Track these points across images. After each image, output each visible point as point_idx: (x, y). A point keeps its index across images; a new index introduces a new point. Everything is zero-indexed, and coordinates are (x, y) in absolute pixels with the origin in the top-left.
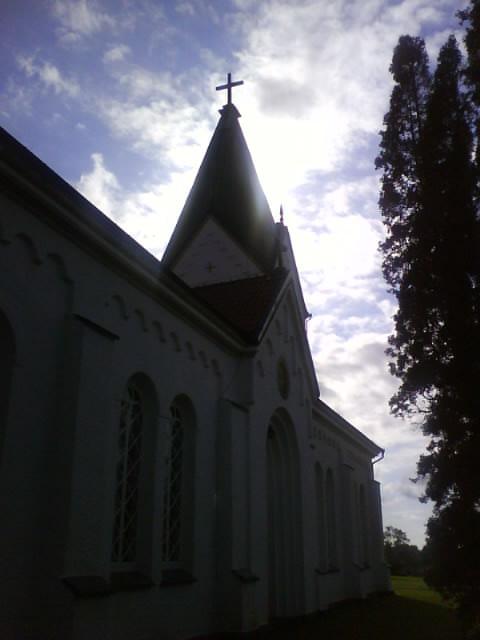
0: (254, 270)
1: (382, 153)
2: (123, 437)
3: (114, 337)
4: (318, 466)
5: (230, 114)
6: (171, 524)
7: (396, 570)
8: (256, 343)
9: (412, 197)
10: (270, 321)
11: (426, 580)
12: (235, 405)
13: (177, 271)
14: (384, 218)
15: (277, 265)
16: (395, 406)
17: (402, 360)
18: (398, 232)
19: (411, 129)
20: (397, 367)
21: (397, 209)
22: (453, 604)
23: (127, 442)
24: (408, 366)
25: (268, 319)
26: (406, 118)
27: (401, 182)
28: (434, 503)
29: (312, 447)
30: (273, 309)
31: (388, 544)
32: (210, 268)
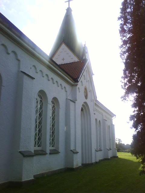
0: (76, 59)
1: (120, 15)
2: (36, 134)
3: (33, 78)
4: (96, 119)
5: (69, 10)
6: (52, 136)
7: (119, 151)
8: (78, 82)
9: (130, 31)
10: (82, 75)
11: (131, 153)
12: (71, 100)
13: (54, 59)
14: (121, 37)
15: (84, 58)
16: (123, 99)
17: (126, 84)
18: (125, 42)
19: (130, 8)
20: (124, 86)
21: (125, 35)
22: (140, 160)
23: (38, 112)
24: (127, 86)
25: (81, 75)
26: (129, 4)
27: (126, 26)
28: (135, 129)
29: (95, 114)
30: (83, 71)
31: (116, 143)
32: (63, 59)
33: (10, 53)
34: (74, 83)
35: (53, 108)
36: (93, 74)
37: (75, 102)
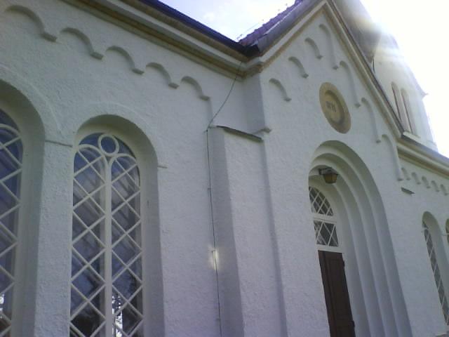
12: (227, 130)
33: (142, 70)
34: (242, 61)
35: (311, 198)
36: (423, 94)
37: (255, 138)
